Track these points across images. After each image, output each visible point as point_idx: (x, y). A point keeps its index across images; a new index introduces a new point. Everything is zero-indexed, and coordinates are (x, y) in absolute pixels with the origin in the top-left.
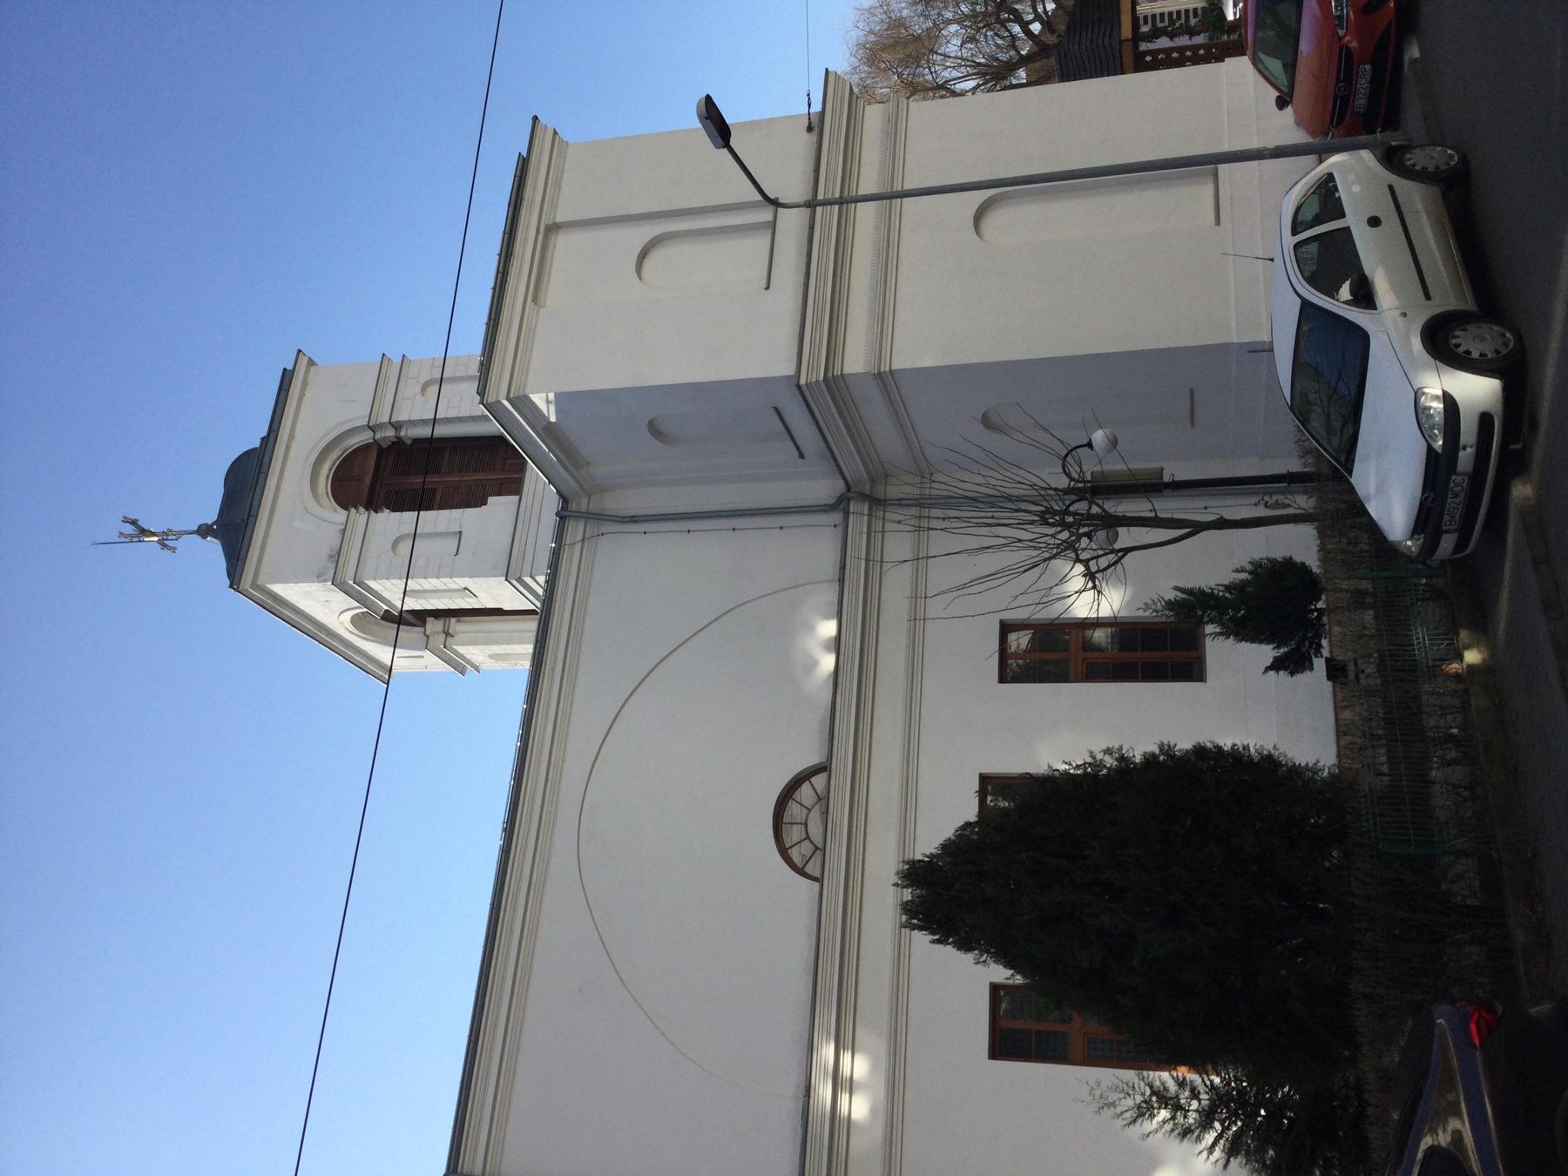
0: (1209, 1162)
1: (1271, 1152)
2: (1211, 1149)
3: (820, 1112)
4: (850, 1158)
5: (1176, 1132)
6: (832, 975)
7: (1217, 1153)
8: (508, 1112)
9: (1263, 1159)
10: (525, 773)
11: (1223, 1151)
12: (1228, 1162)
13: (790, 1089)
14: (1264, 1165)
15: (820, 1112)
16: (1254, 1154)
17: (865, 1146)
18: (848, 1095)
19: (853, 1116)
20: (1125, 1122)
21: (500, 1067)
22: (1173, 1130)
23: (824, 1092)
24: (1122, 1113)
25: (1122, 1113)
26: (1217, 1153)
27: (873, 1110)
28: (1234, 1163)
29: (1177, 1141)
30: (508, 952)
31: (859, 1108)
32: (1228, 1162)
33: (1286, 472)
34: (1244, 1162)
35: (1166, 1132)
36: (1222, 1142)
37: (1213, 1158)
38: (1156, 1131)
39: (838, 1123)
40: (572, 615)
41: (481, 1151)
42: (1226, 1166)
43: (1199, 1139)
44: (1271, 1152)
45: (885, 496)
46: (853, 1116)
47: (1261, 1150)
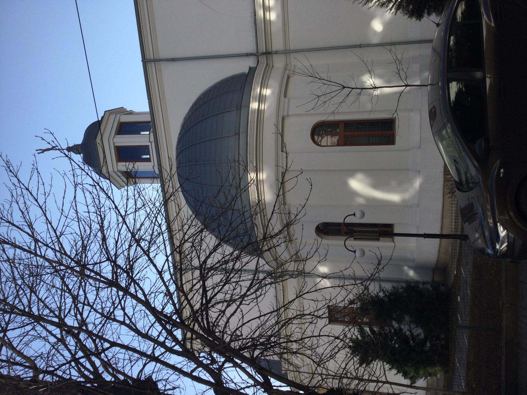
0: (390, 14)
1: (411, 7)
2: (391, 9)
3: (260, 19)
4: (272, 33)
5: (380, 5)
6: (262, 35)
7: (393, 10)
8: (154, 16)
9: (408, 9)
10: (148, 72)
11: (395, 9)
12: (396, 12)
13: (250, 11)
14: (409, 11)
15: (260, 19)
16: (405, 8)
17: (276, 29)
18: (268, 12)
19: (270, 5)
20: (362, 5)
21: (149, 24)
22: (379, 5)
23: (260, 13)
24: (362, 2)
25: (362, 2)
26: (393, 10)
27: (278, 16)
28: (399, 12)
29: (380, 8)
30: (146, 24)
31: (273, 16)
32: (396, 12)
33: (423, 233)
34: (402, 11)
35: (376, 5)
36: (395, 6)
37: (391, 12)
38: (373, 6)
39: (266, 22)
40: (157, 82)
41: (151, 51)
42: (395, 14)
43: (387, 6)
44: (411, 7)
45: (272, 50)
46: (270, 6)
47: (408, 6)
